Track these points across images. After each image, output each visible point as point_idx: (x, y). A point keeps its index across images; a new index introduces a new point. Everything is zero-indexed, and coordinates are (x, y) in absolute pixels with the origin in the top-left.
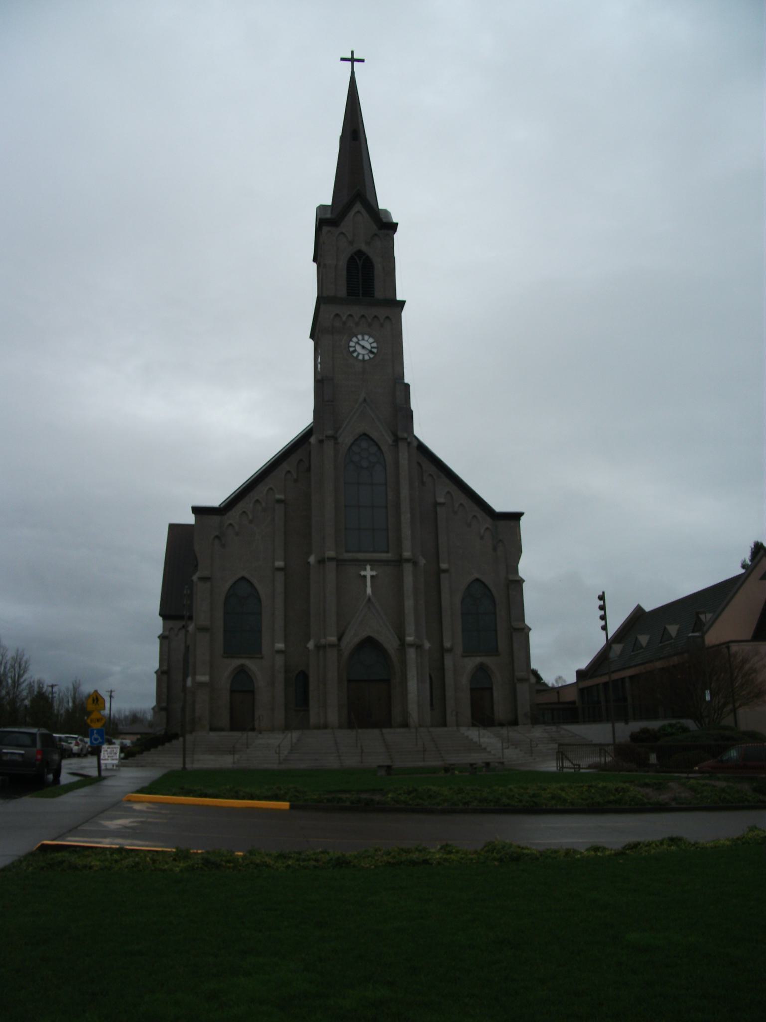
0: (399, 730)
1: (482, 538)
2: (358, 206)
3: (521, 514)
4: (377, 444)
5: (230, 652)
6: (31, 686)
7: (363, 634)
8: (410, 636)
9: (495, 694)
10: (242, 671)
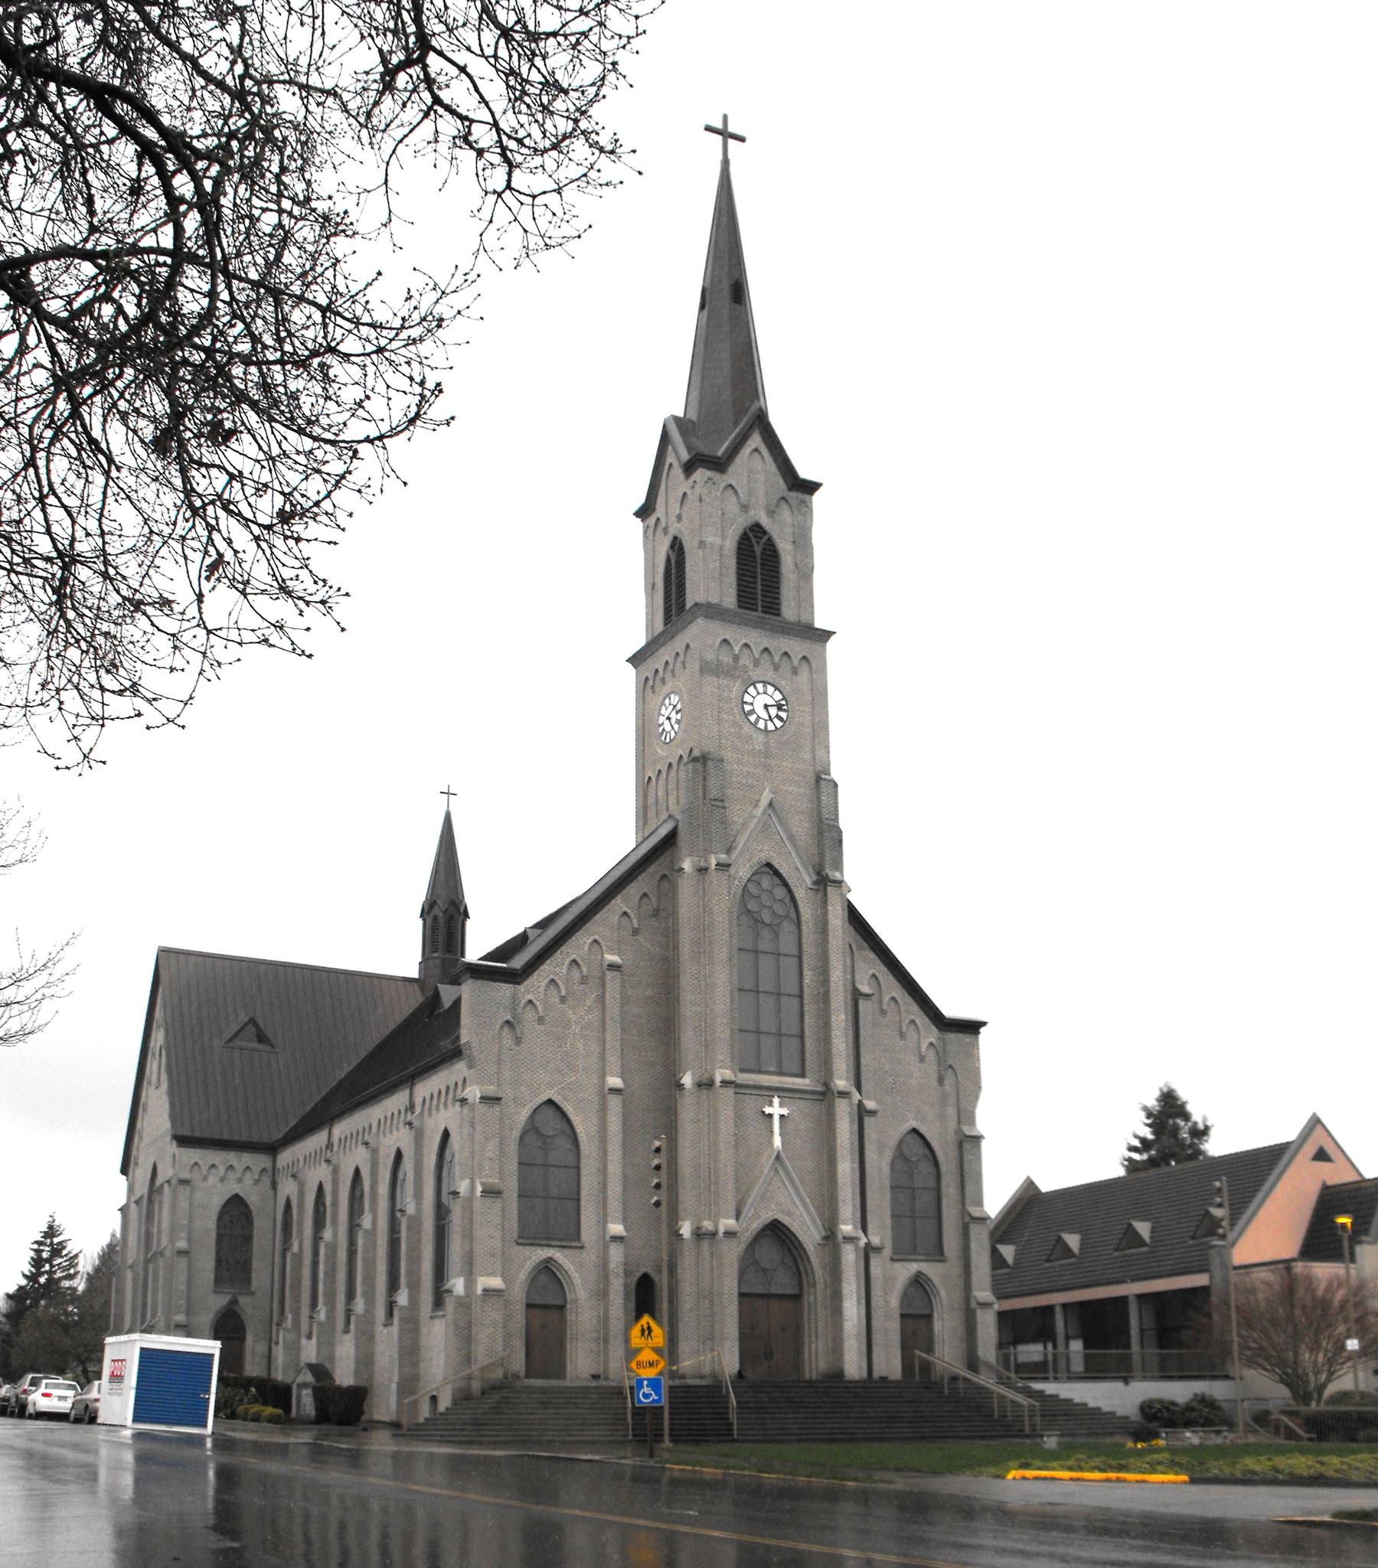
0: (265, 1424)
1: (922, 1059)
2: (756, 440)
3: (984, 1024)
4: (786, 884)
5: (528, 1237)
6: (454, 1285)
7: (767, 1216)
8: (846, 1224)
9: (937, 1326)
10: (547, 1268)
